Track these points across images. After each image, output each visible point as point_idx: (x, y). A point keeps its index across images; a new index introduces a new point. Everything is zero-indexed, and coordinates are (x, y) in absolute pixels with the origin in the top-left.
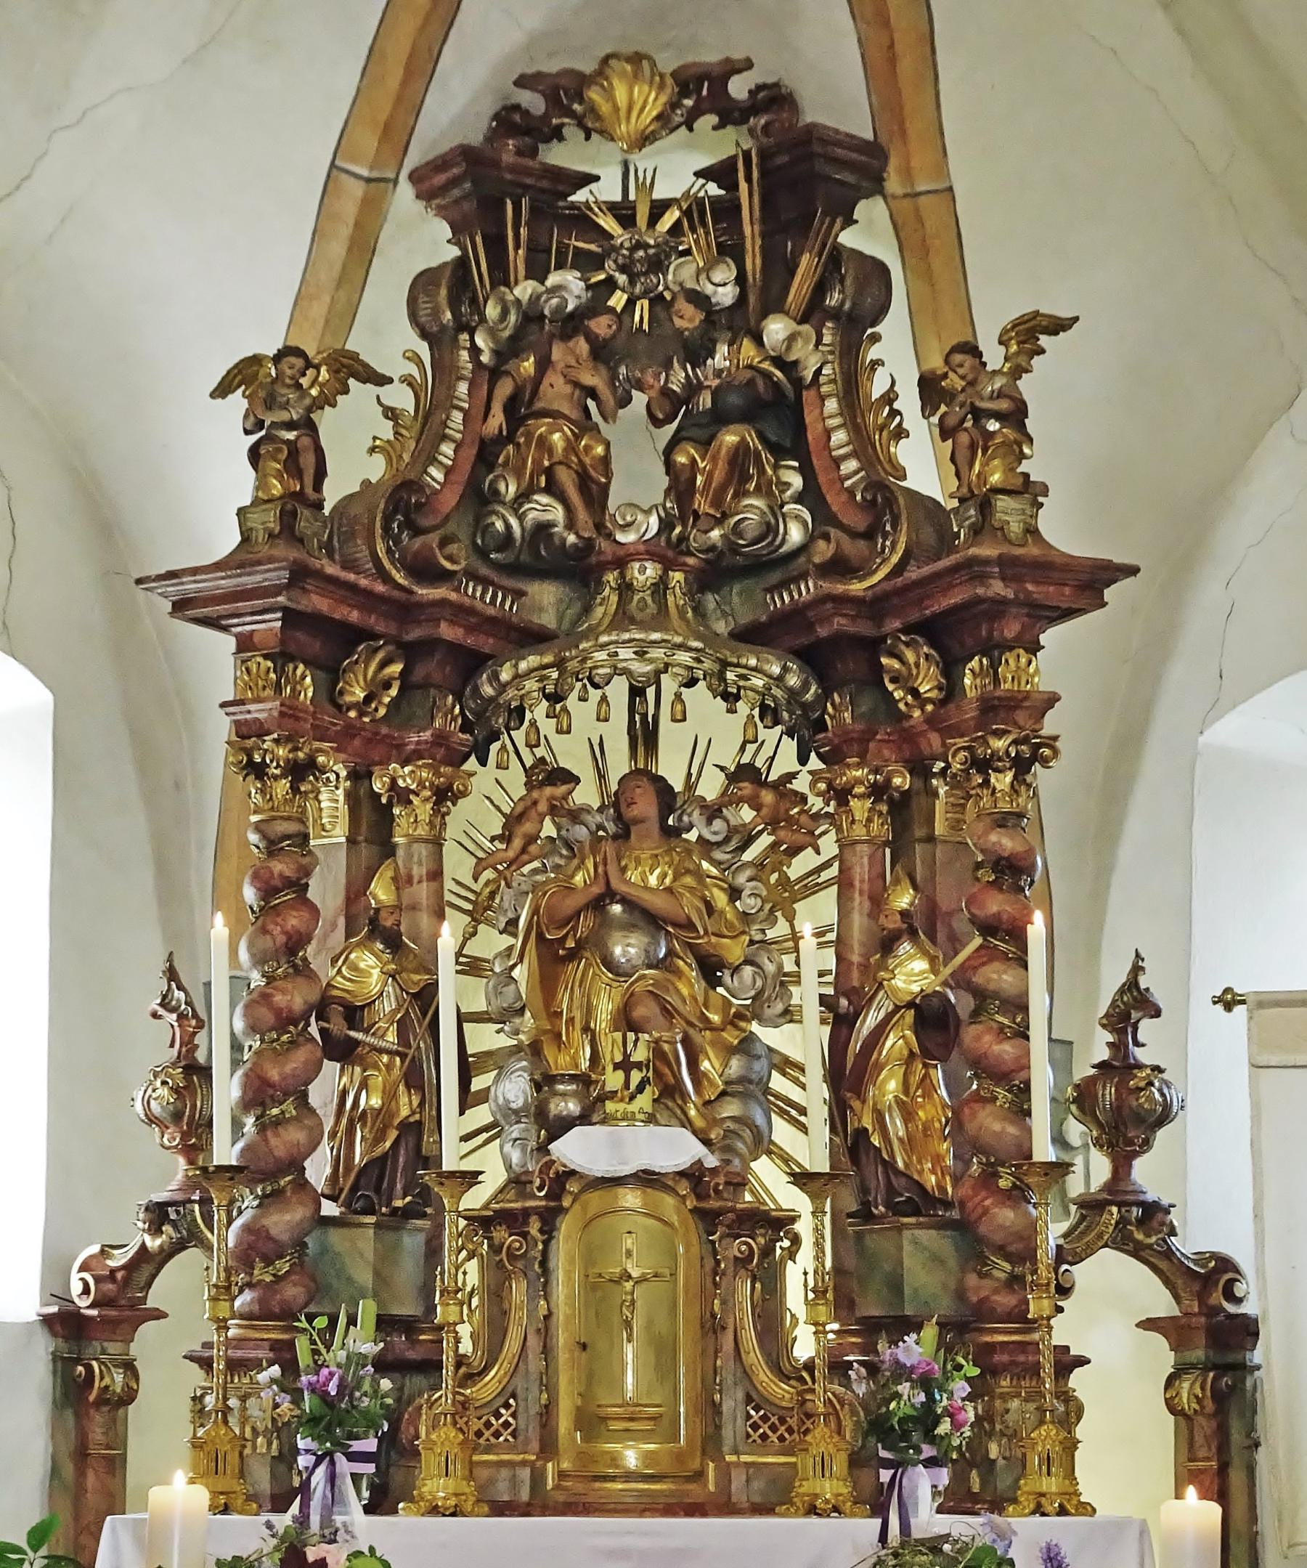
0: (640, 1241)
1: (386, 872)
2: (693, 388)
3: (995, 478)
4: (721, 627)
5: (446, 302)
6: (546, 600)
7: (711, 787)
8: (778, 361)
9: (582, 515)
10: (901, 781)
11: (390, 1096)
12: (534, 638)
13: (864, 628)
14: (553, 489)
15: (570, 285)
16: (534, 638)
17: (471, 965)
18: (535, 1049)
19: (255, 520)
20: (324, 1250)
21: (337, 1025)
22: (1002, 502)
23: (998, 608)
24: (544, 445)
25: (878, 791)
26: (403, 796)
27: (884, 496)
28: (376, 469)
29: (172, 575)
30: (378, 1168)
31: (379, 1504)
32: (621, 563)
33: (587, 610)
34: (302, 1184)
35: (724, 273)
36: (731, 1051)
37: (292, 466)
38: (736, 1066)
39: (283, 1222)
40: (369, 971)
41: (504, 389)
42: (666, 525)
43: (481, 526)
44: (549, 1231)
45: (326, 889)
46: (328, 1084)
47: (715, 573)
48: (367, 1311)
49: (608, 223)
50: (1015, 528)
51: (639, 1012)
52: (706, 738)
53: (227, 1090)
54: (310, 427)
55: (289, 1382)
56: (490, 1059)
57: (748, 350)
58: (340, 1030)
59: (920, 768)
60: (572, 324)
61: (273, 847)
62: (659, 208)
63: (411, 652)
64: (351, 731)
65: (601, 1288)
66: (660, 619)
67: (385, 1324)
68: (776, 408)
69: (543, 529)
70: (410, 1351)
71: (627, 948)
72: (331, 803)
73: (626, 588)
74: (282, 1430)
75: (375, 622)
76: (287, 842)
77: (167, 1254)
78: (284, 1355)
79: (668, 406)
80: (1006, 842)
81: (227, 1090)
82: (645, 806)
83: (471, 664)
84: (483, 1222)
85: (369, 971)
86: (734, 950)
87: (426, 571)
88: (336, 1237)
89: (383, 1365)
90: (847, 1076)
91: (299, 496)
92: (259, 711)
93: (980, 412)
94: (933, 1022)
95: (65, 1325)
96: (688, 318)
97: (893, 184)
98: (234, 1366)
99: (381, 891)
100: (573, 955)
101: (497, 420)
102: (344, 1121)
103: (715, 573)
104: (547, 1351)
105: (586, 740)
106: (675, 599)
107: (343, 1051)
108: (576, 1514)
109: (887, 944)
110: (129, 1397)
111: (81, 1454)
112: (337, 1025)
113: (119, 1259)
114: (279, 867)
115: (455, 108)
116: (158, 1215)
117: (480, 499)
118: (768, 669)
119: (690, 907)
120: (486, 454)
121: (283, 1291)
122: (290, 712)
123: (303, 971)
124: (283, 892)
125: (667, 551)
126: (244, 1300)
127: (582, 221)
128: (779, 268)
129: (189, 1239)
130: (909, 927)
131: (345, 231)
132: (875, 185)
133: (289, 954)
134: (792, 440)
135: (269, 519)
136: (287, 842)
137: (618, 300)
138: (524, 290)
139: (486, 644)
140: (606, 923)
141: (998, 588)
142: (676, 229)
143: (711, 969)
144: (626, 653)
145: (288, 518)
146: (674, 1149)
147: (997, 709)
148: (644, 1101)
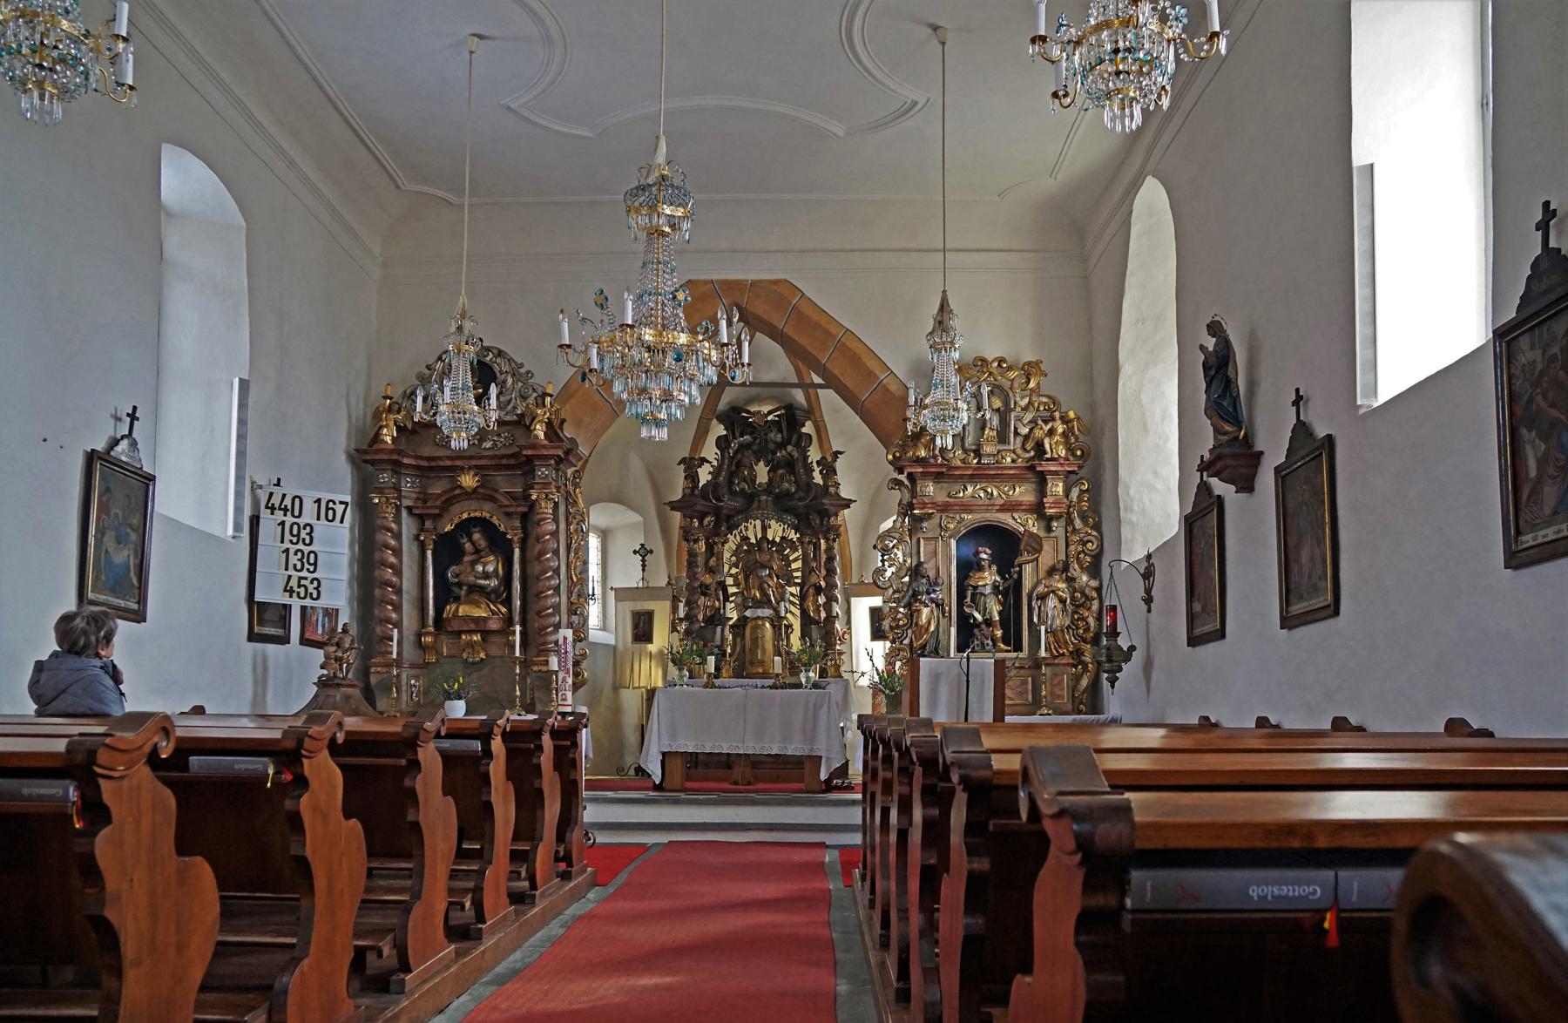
5: (722, 443)
17: (730, 573)
27: (809, 484)
40: (708, 579)
45: (700, 560)
76: (692, 555)
93: (829, 470)
102: (449, 463)
107: (705, 594)
108: (1363, 851)
117: (730, 483)
124: (691, 564)
128: (790, 438)
133: (692, 575)
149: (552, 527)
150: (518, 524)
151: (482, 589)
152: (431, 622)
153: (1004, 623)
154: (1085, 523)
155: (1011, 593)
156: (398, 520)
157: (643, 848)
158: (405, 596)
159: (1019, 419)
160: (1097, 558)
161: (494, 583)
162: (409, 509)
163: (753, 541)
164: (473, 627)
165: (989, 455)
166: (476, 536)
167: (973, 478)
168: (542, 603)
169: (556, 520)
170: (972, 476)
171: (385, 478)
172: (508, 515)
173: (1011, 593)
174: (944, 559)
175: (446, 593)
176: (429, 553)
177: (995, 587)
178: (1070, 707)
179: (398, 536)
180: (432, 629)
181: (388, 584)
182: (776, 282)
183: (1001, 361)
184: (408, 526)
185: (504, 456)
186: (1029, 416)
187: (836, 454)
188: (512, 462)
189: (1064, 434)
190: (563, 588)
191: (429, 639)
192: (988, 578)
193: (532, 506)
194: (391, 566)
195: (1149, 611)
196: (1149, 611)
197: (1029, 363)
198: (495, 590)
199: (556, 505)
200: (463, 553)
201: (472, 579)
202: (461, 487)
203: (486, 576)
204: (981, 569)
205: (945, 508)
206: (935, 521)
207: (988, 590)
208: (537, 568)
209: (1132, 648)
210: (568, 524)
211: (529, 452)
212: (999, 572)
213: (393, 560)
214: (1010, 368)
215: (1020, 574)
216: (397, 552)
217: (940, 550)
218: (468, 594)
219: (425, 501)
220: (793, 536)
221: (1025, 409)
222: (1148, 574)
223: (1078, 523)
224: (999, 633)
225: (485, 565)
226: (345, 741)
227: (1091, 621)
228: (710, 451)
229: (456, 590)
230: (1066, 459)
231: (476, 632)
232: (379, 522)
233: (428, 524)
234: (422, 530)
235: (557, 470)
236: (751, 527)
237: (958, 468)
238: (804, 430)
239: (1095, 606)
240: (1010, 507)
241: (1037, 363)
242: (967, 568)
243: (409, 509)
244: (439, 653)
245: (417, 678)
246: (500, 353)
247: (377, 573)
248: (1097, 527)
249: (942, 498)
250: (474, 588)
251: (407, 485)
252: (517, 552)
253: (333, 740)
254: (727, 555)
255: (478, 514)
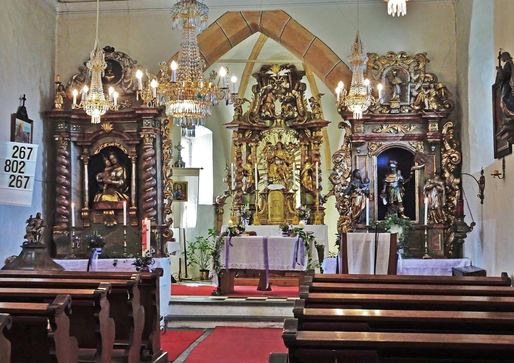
0: (279, 196)
1: (250, 156)
2: (284, 98)
3: (316, 112)
4: (288, 125)
5: (256, 89)
6: (268, 122)
7: (287, 144)
8: (294, 95)
9: (272, 114)
10: (308, 144)
11: (251, 180)
12: (267, 128)
13: (303, 127)
14: (268, 111)
15: (270, 86)
16: (267, 128)
18: (268, 174)
19: (235, 118)
20: (244, 197)
21: (245, 173)
22: (316, 115)
23: (316, 127)
24: (267, 106)
25: (305, 145)
26: (252, 146)
28: (249, 109)
29: (226, 124)
30: (250, 188)
31: (250, 224)
32: (276, 119)
33: (273, 124)
34: (242, 190)
35: (288, 84)
36: (290, 174)
37: (239, 112)
38: (290, 175)
39: (240, 194)
40: (248, 167)
41: (263, 99)
42: (282, 114)
43: (260, 115)
44: (268, 195)
46: (244, 179)
47: (287, 119)
48: (248, 204)
49: (274, 78)
50: (318, 118)
51: (279, 170)
52: (288, 138)
53: (233, 180)
54: (241, 106)
55: (240, 212)
56: (262, 175)
57: (290, 94)
58: (246, 173)
59: (310, 142)
60: (271, 91)
61: (238, 154)
62: (280, 77)
63: (252, 131)
64: (246, 139)
65: (273, 202)
66: (280, 126)
67: (250, 205)
68: (293, 101)
69: (267, 115)
70: (253, 208)
71: (278, 162)
72: (244, 147)
73: (277, 122)
74: (240, 217)
75: (248, 128)
77: (227, 197)
78: (240, 209)
79: (281, 100)
80: (317, 152)
81: (233, 180)
82: (280, 146)
83: (260, 131)
84: (261, 194)
85: (248, 167)
86: (290, 162)
87: (254, 122)
88: (246, 196)
89: (250, 210)
90: (301, 177)
91: (240, 115)
92: (236, 139)
94: (310, 172)
95: (216, 205)
96: (283, 90)
97: (306, 74)
98: (235, 210)
99: (249, 158)
100: (272, 163)
101: (262, 103)
103: (287, 119)
104: (268, 208)
105: (273, 138)
106: (283, 123)
107: (246, 176)
109: (305, 163)
110: (223, 213)
111: (218, 220)
112: (245, 173)
113: (222, 197)
114: (238, 156)
115: (257, 68)
116: (226, 193)
117: (260, 111)
118: (293, 131)
119: (285, 158)
120: (261, 107)
121: (241, 201)
122: (239, 139)
123: (241, 167)
125: (282, 117)
126: (236, 203)
127: (271, 79)
129: (230, 195)
130: (307, 161)
131: (244, 81)
132: (305, 75)
133: (240, 165)
134: (295, 105)
135: (236, 118)
136: (239, 153)
137: (275, 88)
138: (265, 87)
139: (261, 129)
140: (275, 160)
141: (315, 125)
142: (282, 79)
143: (288, 165)
144: (276, 130)
145: (238, 118)
146: (281, 186)
147: (317, 138)
148: (277, 182)
149: (151, 152)
150: (134, 150)
151: (115, 186)
152: (86, 203)
153: (404, 204)
154: (452, 147)
155: (408, 186)
156: (69, 149)
157: (201, 331)
158: (73, 191)
159: (412, 87)
160: (459, 166)
161: (121, 182)
162: (75, 143)
163: (274, 144)
164: (109, 207)
165: (395, 109)
166: (112, 157)
167: (386, 122)
168: (147, 194)
169: (154, 148)
170: (386, 121)
171: (61, 126)
172: (129, 145)
173: (408, 186)
174: (369, 167)
175: (96, 187)
176: (86, 166)
177: (400, 182)
178: (442, 253)
179: (68, 158)
180: (87, 208)
181: (64, 184)
182: (276, 12)
183: (402, 54)
184: (74, 152)
185: (126, 113)
186: (418, 86)
187: (320, 95)
188: (131, 116)
189: (436, 96)
190: (159, 185)
191: (86, 214)
192: (394, 179)
193: (142, 140)
194: (65, 175)
195: (482, 203)
196: (482, 203)
197: (418, 55)
198: (122, 186)
199: (155, 140)
200: (105, 166)
201: (109, 180)
202: (103, 130)
203: (117, 178)
204: (391, 172)
205: (370, 139)
206: (365, 146)
207: (395, 185)
208: (144, 176)
209: (473, 224)
210: (162, 149)
211: (140, 112)
212: (402, 174)
213: (66, 171)
214: (408, 58)
215: (414, 175)
216: (68, 167)
217: (367, 163)
218: (107, 188)
219: (83, 138)
220: (296, 141)
221: (417, 81)
222: (482, 182)
223: (448, 147)
224: (402, 209)
225: (117, 172)
226: (11, 329)
227: (455, 202)
228: (249, 95)
229: (101, 186)
230: (438, 110)
231: (111, 210)
232: (59, 150)
233: (85, 151)
234: (82, 154)
235: (155, 121)
236: (272, 137)
237: (378, 116)
238: (302, 81)
239: (458, 194)
240: (407, 138)
241: (424, 55)
242: (383, 172)
243: (74, 142)
244: (91, 222)
245: (79, 235)
246: (124, 56)
247: (58, 178)
248: (459, 149)
249: (369, 133)
250: (110, 185)
251: (73, 129)
252: (134, 165)
253: (5, 329)
254: (259, 152)
255: (112, 144)
